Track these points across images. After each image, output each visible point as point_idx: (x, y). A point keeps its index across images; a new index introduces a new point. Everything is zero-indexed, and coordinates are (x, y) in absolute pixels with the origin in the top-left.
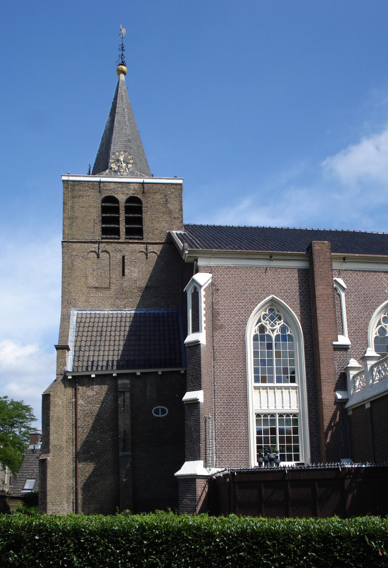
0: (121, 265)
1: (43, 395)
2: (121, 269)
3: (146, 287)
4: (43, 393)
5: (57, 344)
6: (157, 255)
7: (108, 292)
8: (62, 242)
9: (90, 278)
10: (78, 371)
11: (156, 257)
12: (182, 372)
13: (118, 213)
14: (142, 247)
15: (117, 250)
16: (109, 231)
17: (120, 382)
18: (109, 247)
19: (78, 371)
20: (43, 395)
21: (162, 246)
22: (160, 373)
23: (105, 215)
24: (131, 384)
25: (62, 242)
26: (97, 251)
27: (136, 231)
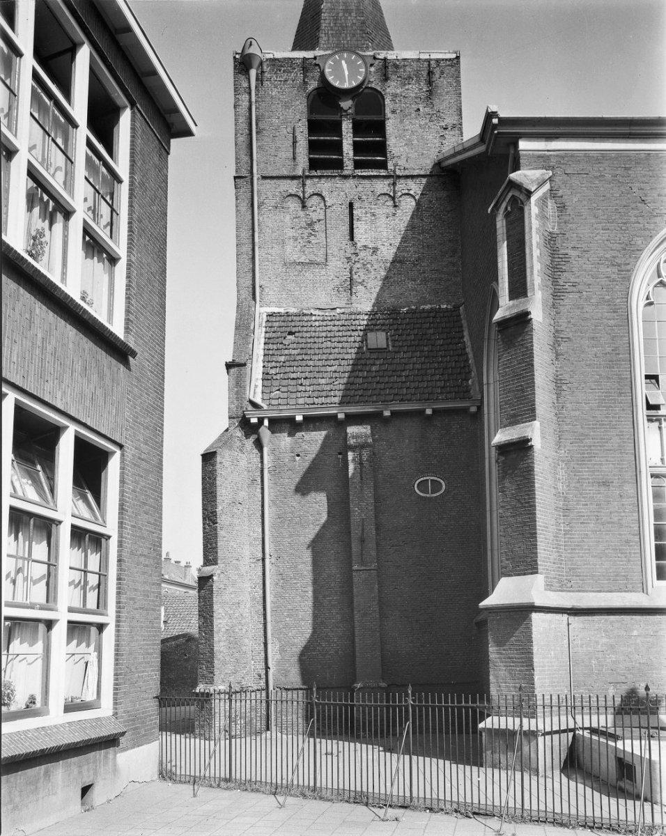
0: (347, 220)
1: (202, 455)
2: (346, 228)
3: (393, 262)
4: (202, 453)
5: (230, 359)
6: (415, 200)
7: (323, 272)
8: (235, 178)
9: (289, 249)
10: (53, 176)
11: (414, 203)
12: (473, 409)
13: (340, 135)
14: (382, 186)
15: (336, 191)
16: (324, 158)
17: (352, 430)
18: (324, 186)
19: (53, 176)
20: (202, 455)
21: (424, 181)
22: (429, 412)
23: (312, 156)
24: (373, 434)
25: (235, 178)
26: (301, 195)
27: (373, 152)
